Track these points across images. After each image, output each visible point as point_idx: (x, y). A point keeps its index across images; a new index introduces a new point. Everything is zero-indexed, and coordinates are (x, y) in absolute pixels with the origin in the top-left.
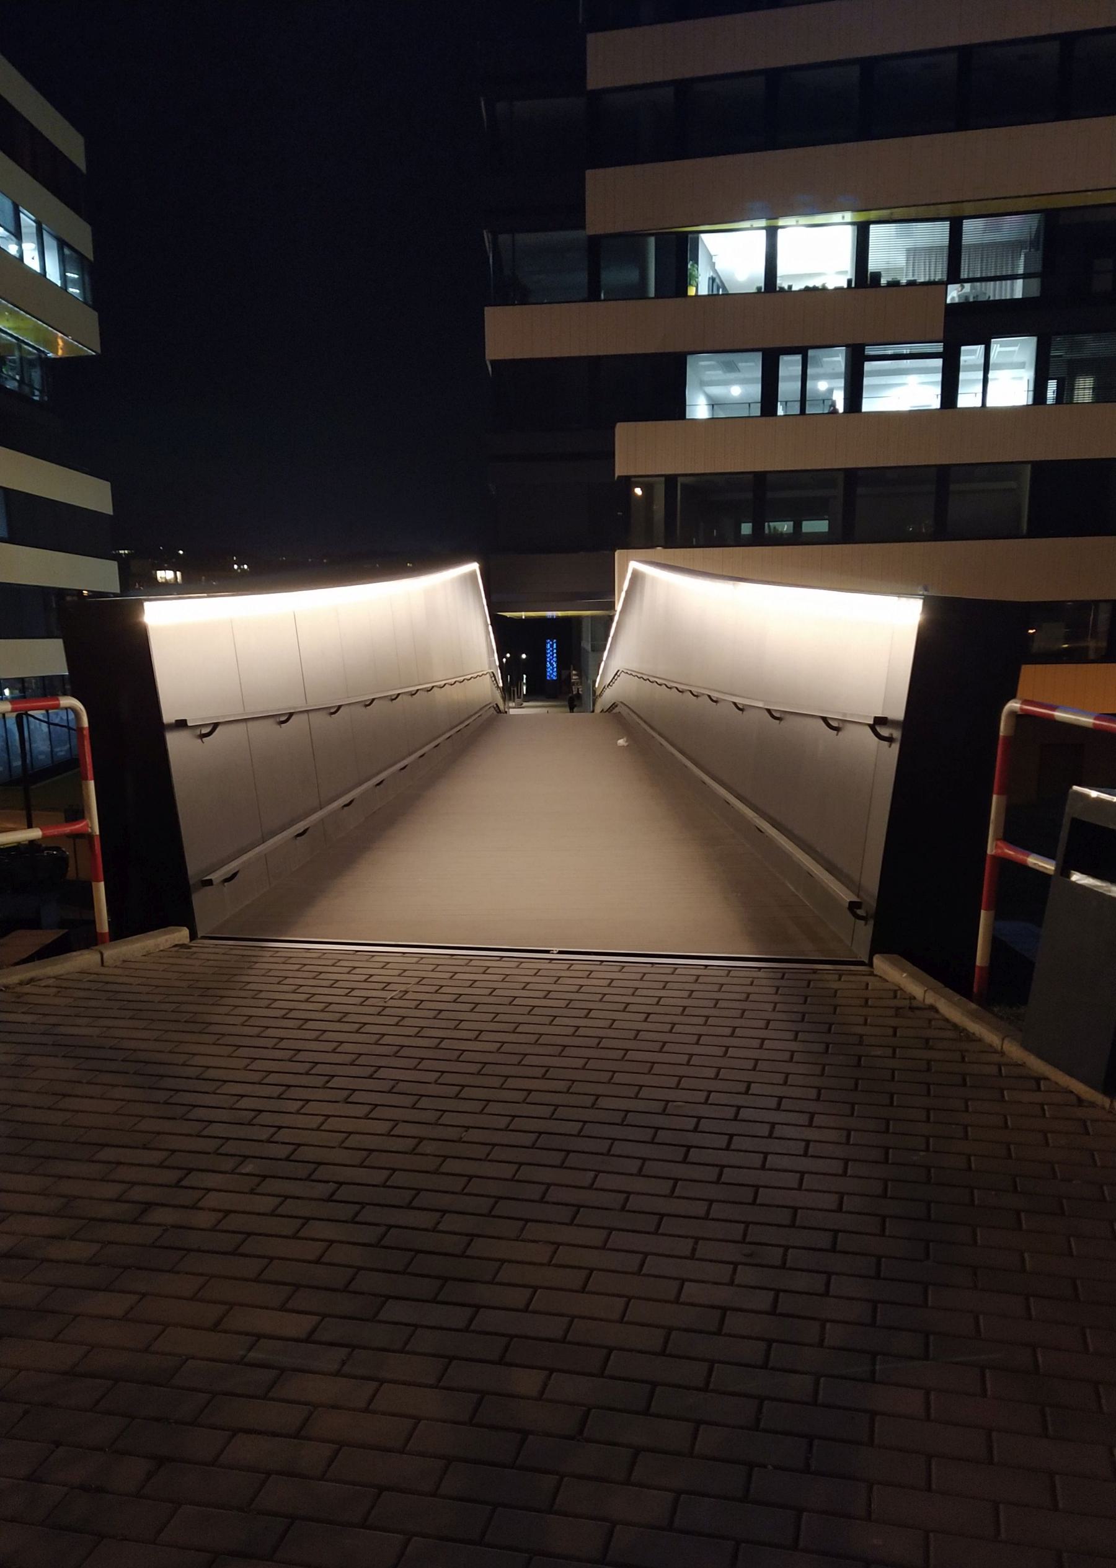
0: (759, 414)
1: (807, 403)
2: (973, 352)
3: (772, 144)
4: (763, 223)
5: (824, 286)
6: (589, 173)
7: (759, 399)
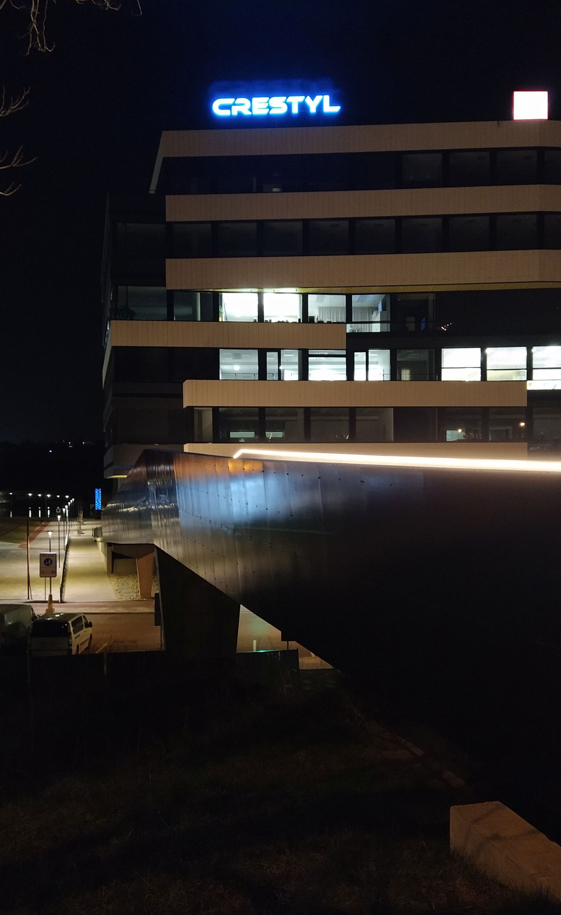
0: (277, 379)
1: (267, 374)
2: (273, 356)
3: (260, 254)
4: (256, 290)
5: (287, 321)
6: (168, 261)
7: (258, 373)
